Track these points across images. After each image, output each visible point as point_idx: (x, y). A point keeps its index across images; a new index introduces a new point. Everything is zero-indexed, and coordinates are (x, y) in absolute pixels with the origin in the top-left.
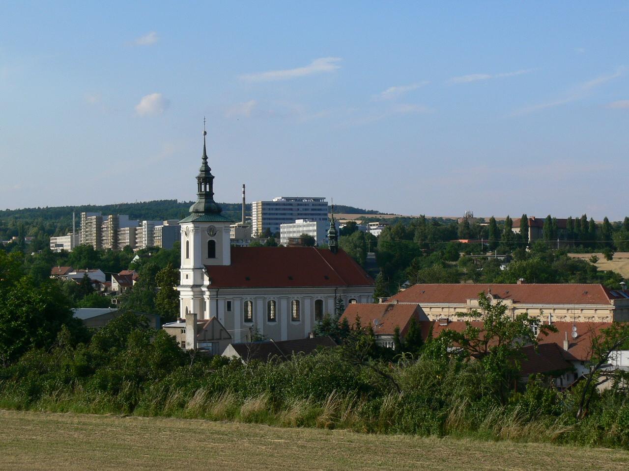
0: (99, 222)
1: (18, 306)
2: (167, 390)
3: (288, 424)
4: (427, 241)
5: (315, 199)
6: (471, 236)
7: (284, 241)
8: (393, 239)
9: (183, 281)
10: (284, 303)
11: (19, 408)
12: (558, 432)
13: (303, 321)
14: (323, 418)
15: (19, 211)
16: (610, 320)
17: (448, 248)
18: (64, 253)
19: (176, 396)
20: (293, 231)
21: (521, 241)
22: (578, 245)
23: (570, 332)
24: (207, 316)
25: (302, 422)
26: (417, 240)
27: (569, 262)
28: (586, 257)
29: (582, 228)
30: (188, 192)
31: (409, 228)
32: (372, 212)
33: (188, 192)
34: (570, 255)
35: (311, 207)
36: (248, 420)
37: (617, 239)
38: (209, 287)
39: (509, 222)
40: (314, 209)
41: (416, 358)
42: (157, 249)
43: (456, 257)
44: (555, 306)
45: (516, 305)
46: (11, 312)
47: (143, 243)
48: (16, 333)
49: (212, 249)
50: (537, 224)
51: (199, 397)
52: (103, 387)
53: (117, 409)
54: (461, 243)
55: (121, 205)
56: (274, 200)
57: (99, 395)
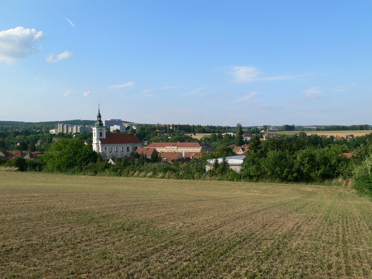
0: (63, 126)
1: (86, 152)
2: (129, 171)
3: (159, 178)
4: (149, 131)
5: (119, 120)
6: (160, 129)
7: (111, 131)
8: (140, 130)
9: (94, 142)
10: (113, 148)
11: (93, 176)
12: (218, 178)
13: (118, 152)
14: (166, 177)
15: (38, 123)
16: (200, 151)
17: (155, 132)
18: (54, 134)
19: (131, 173)
20: (114, 128)
21: (172, 131)
22: (186, 132)
23: (192, 154)
24: (100, 151)
25: (161, 178)
26: (146, 130)
27: (186, 136)
28: (189, 135)
29: (187, 127)
30: (95, 119)
31: (144, 128)
32: (132, 123)
33: (95, 119)
34: (185, 134)
35: (118, 122)
36: (149, 177)
37: (196, 130)
38: (100, 144)
39: (169, 126)
40: (119, 122)
41: (183, 164)
42: (79, 133)
43: (157, 135)
44: (187, 148)
45: (178, 148)
46: (85, 154)
47: (75, 131)
48: (86, 158)
49: (101, 134)
50: (176, 126)
51: (137, 173)
52: (113, 171)
53: (117, 175)
54: (157, 131)
55: (66, 121)
56: (108, 120)
57: (113, 173)
